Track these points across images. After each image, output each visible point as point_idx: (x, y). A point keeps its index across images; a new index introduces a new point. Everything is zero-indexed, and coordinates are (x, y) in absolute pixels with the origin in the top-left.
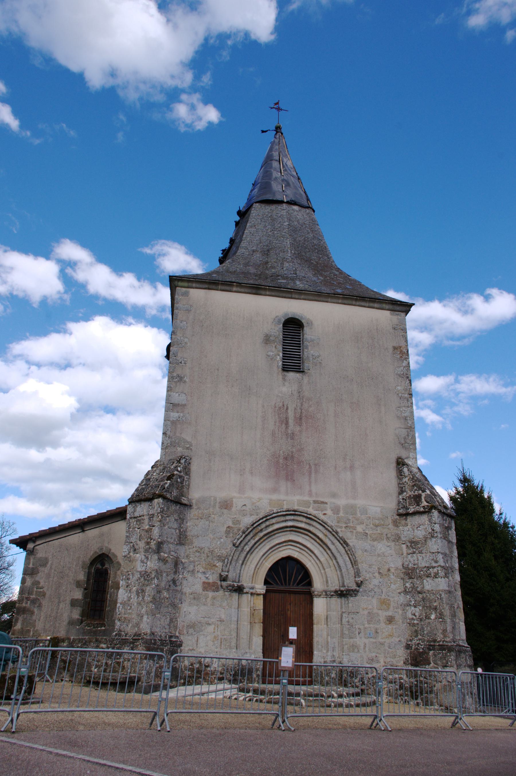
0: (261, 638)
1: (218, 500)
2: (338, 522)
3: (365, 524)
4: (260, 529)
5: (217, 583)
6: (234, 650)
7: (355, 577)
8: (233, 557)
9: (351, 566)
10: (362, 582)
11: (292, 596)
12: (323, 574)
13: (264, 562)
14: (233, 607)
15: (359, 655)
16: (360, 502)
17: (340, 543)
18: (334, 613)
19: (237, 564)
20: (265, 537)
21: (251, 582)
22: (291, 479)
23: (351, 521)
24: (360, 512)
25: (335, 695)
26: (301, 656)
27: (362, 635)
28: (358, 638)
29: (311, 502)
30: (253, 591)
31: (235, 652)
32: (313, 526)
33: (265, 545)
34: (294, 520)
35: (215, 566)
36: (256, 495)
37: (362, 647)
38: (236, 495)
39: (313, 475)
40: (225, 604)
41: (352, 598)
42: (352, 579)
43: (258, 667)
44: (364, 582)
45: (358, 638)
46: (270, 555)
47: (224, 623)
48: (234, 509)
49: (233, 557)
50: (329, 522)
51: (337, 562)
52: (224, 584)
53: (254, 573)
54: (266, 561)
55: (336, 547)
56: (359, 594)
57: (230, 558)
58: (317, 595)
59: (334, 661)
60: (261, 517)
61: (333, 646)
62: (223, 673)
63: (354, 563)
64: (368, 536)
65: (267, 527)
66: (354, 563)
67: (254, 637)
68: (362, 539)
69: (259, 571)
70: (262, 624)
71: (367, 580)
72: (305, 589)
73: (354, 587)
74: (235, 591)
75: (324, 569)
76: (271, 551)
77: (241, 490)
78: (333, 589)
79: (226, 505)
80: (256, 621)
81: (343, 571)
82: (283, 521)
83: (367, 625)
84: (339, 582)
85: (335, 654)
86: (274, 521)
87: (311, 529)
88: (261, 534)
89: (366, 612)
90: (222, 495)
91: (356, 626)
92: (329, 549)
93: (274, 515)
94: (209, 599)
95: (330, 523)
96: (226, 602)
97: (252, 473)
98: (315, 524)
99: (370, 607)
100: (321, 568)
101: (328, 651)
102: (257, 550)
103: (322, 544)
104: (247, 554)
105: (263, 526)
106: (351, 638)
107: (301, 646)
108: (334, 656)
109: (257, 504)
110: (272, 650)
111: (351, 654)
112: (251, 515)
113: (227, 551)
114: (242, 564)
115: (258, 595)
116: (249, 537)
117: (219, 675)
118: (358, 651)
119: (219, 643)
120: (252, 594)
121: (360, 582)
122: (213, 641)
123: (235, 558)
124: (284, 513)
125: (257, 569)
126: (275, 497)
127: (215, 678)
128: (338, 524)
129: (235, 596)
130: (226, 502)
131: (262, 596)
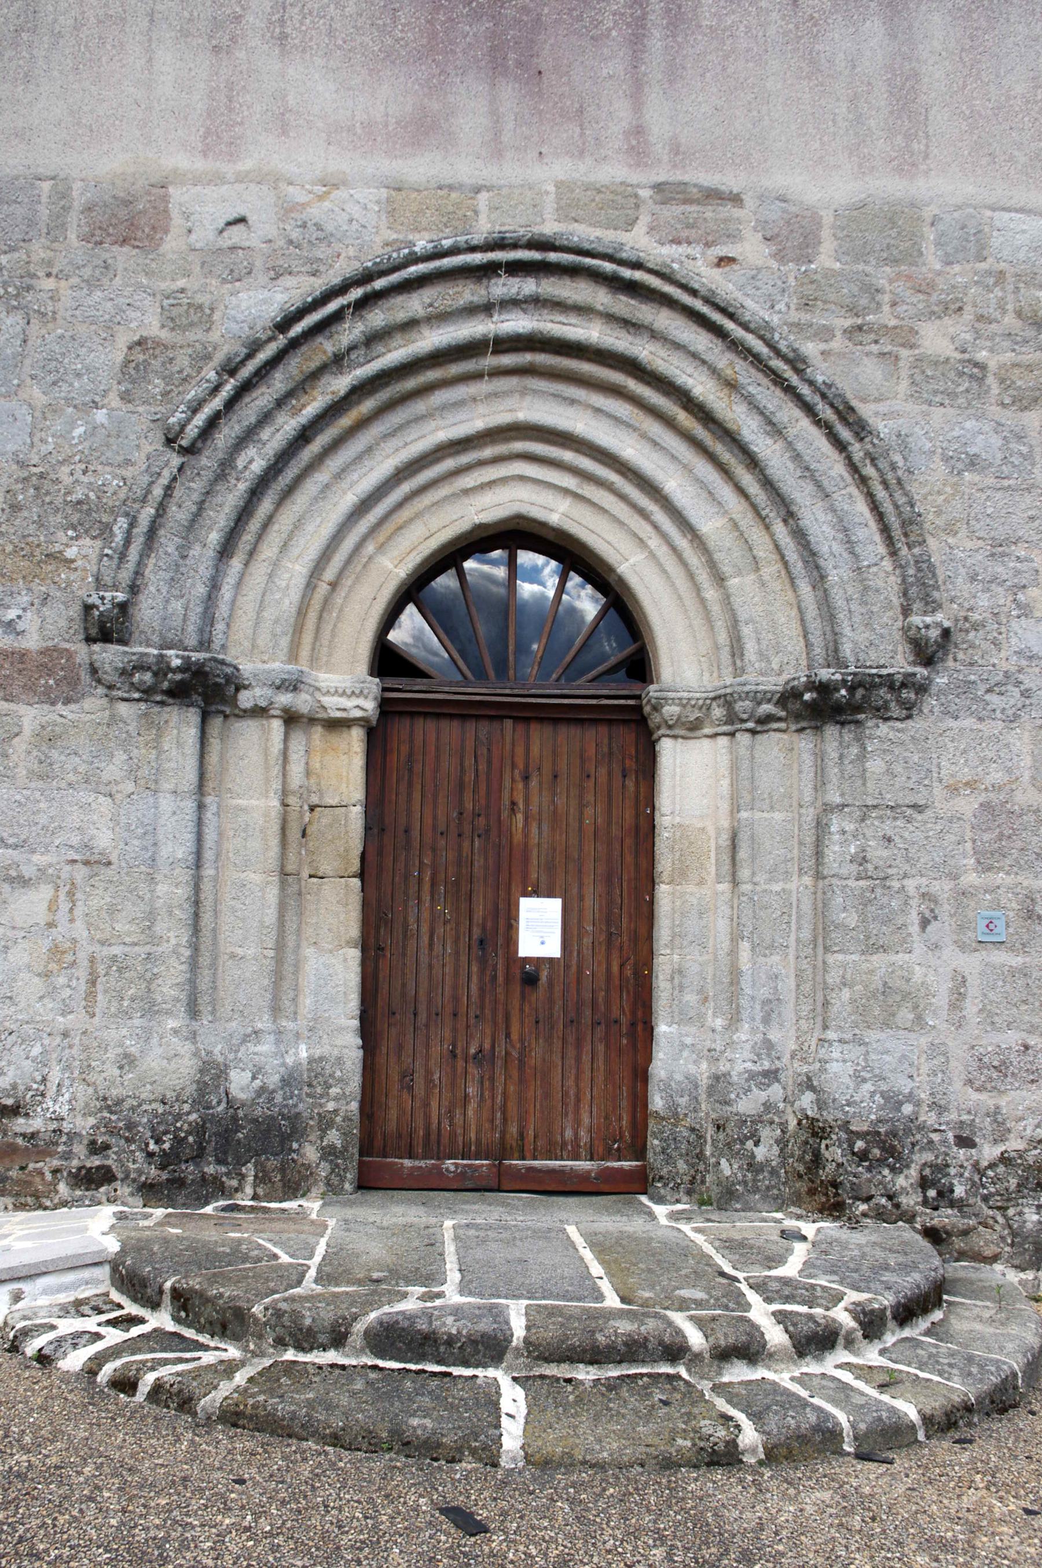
0: (354, 954)
1: (79, 197)
2: (806, 305)
3: (968, 316)
4: (334, 356)
5: (70, 655)
6: (171, 1023)
7: (906, 611)
8: (161, 509)
9: (882, 550)
10: (946, 633)
11: (539, 737)
12: (716, 609)
13: (370, 548)
14: (167, 786)
15: (924, 1041)
16: (944, 188)
17: (818, 422)
18: (778, 816)
19: (196, 551)
20: (368, 405)
21: (282, 654)
22: (519, 64)
23: (887, 298)
24: (938, 244)
25: (776, 1336)
26: (587, 1048)
27: (942, 929)
28: (919, 948)
29: (645, 193)
30: (302, 702)
31: (175, 1032)
32: (655, 335)
33: (369, 450)
34: (537, 302)
35: (56, 557)
36: (305, 159)
37: (942, 1000)
38: (181, 161)
39: (656, 42)
40: (113, 769)
41: (884, 729)
42: (890, 622)
43: (331, 1106)
44: (957, 637)
45: (919, 948)
46: (406, 513)
47: (109, 872)
48: (172, 244)
49: (161, 509)
50: (749, 303)
51: (800, 535)
52: (109, 655)
53: (310, 603)
54: (381, 548)
55: (792, 447)
56: (931, 702)
57: (149, 511)
58: (679, 722)
59: (771, 1076)
60: (337, 280)
61: (764, 993)
62: (106, 1147)
63: (899, 529)
64: (990, 380)
65: (374, 339)
66: (899, 529)
67: (309, 951)
68: (952, 395)
69: (338, 600)
70: (356, 882)
71: (976, 627)
72: (615, 691)
73: (900, 662)
74: (179, 693)
75: (720, 579)
76: (406, 488)
77: (220, 135)
78: (774, 683)
79: (130, 221)
80: (325, 868)
81: (833, 577)
82: (471, 311)
83: (971, 879)
84: (808, 645)
85: (774, 1036)
86: (415, 304)
87: (644, 351)
88: (341, 383)
89: (967, 805)
90: (105, 164)
91: (910, 884)
92: (753, 462)
93: (413, 270)
94: (20, 745)
95: (754, 308)
96: (120, 756)
97: (284, 36)
98: (664, 320)
99: (996, 776)
100: (703, 576)
101: (734, 1020)
102: (321, 477)
103: (710, 434)
104: (255, 493)
105: (350, 332)
106: (874, 948)
107: (587, 995)
108: (769, 1045)
109: (316, 212)
110: (423, 1017)
111: (872, 1036)
112: (277, 274)
113: (128, 472)
114: (225, 551)
115: (336, 725)
116: (262, 398)
117: (81, 1157)
118: (919, 1019)
119: (83, 987)
120: (291, 719)
121: (934, 634)
122: (47, 975)
123: (178, 514)
124: (478, 258)
125: (323, 588)
126: (421, 168)
127: (55, 1172)
128: (805, 317)
129: (182, 725)
130: (127, 203)
131: (356, 737)
